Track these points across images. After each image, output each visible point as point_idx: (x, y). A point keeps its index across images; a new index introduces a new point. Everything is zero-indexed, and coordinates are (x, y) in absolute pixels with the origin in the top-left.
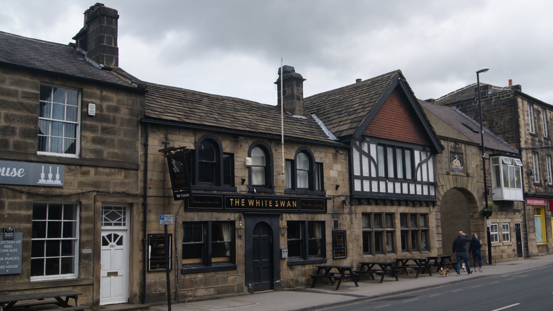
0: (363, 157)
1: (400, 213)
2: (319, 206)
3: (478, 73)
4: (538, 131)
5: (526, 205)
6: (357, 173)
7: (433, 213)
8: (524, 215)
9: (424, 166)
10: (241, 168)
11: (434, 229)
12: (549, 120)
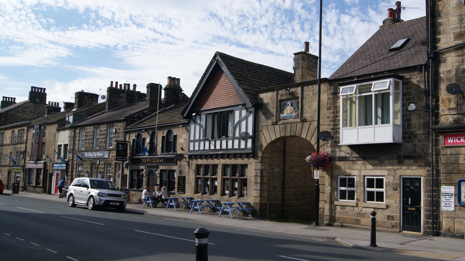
7: (252, 164)
11: (253, 179)
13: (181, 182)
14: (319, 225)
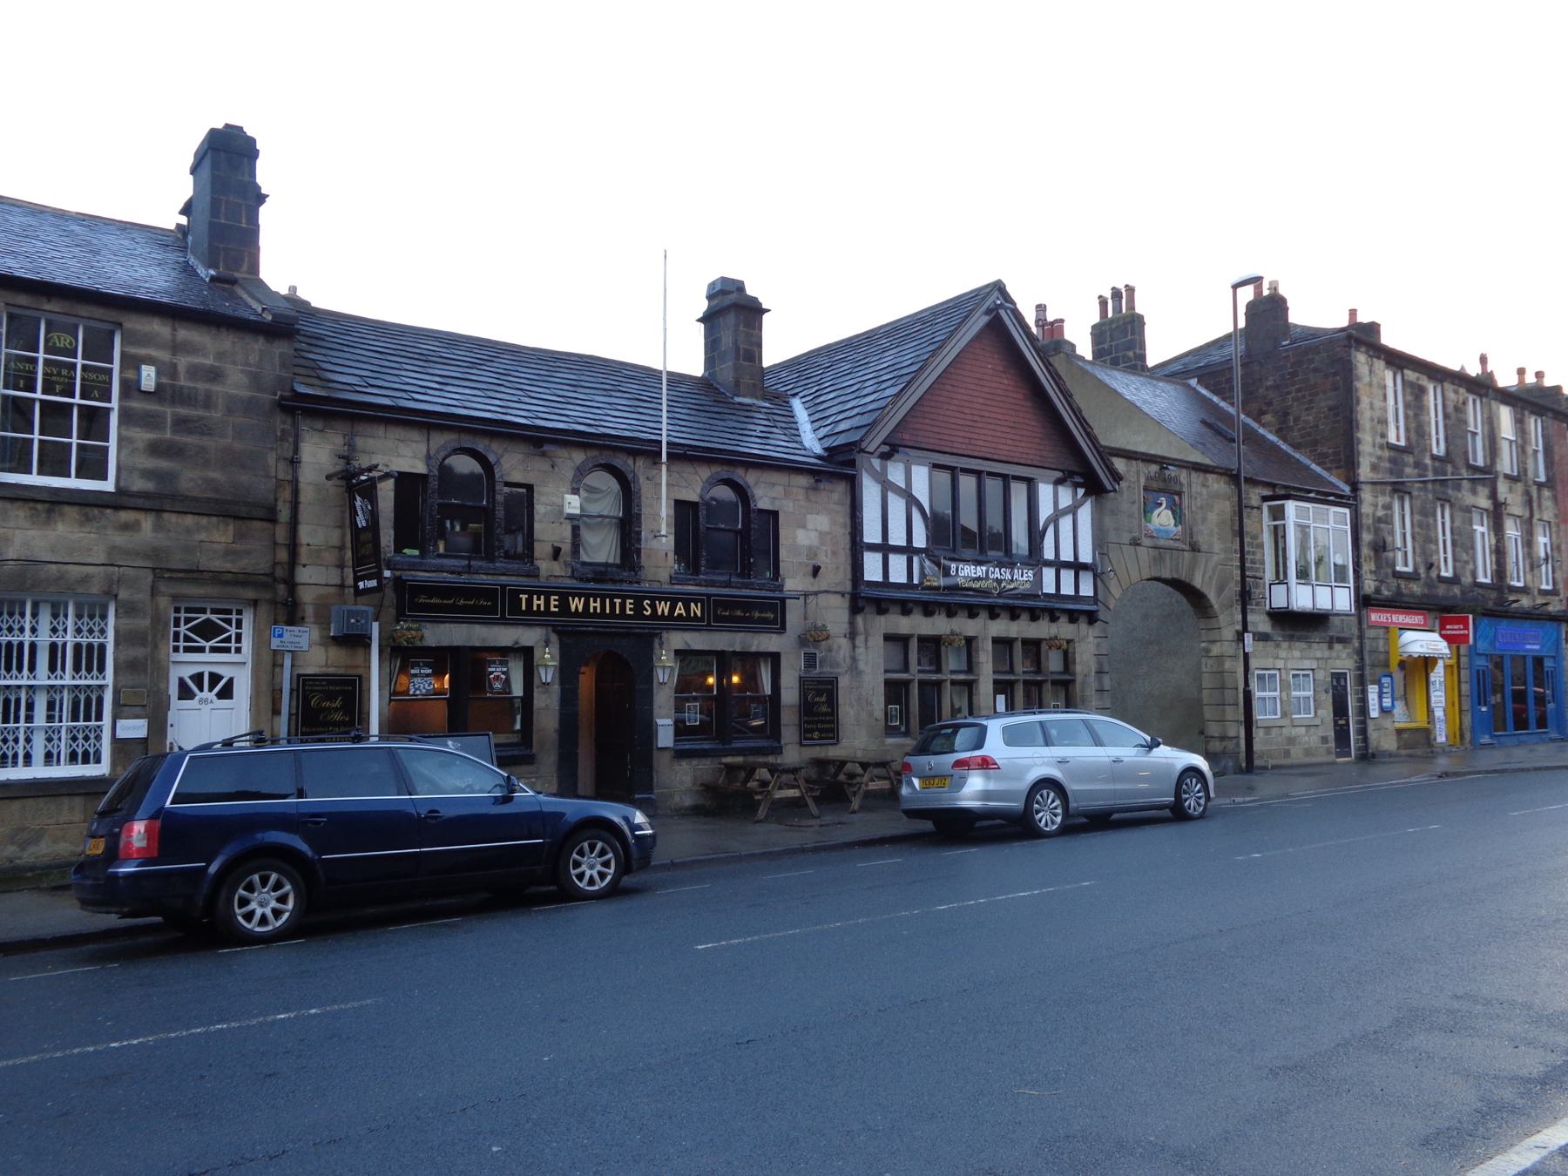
0: (891, 497)
1: (993, 638)
2: (763, 615)
3: (1235, 287)
4: (1413, 437)
5: (1365, 626)
6: (872, 534)
8: (1360, 652)
9: (1066, 524)
10: (552, 520)
11: (1092, 678)
12: (1450, 410)
13: (817, 699)
14: (1254, 771)
